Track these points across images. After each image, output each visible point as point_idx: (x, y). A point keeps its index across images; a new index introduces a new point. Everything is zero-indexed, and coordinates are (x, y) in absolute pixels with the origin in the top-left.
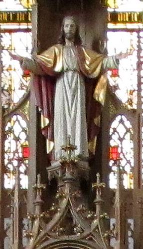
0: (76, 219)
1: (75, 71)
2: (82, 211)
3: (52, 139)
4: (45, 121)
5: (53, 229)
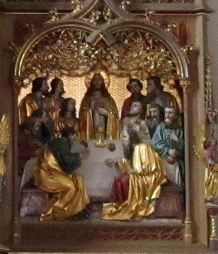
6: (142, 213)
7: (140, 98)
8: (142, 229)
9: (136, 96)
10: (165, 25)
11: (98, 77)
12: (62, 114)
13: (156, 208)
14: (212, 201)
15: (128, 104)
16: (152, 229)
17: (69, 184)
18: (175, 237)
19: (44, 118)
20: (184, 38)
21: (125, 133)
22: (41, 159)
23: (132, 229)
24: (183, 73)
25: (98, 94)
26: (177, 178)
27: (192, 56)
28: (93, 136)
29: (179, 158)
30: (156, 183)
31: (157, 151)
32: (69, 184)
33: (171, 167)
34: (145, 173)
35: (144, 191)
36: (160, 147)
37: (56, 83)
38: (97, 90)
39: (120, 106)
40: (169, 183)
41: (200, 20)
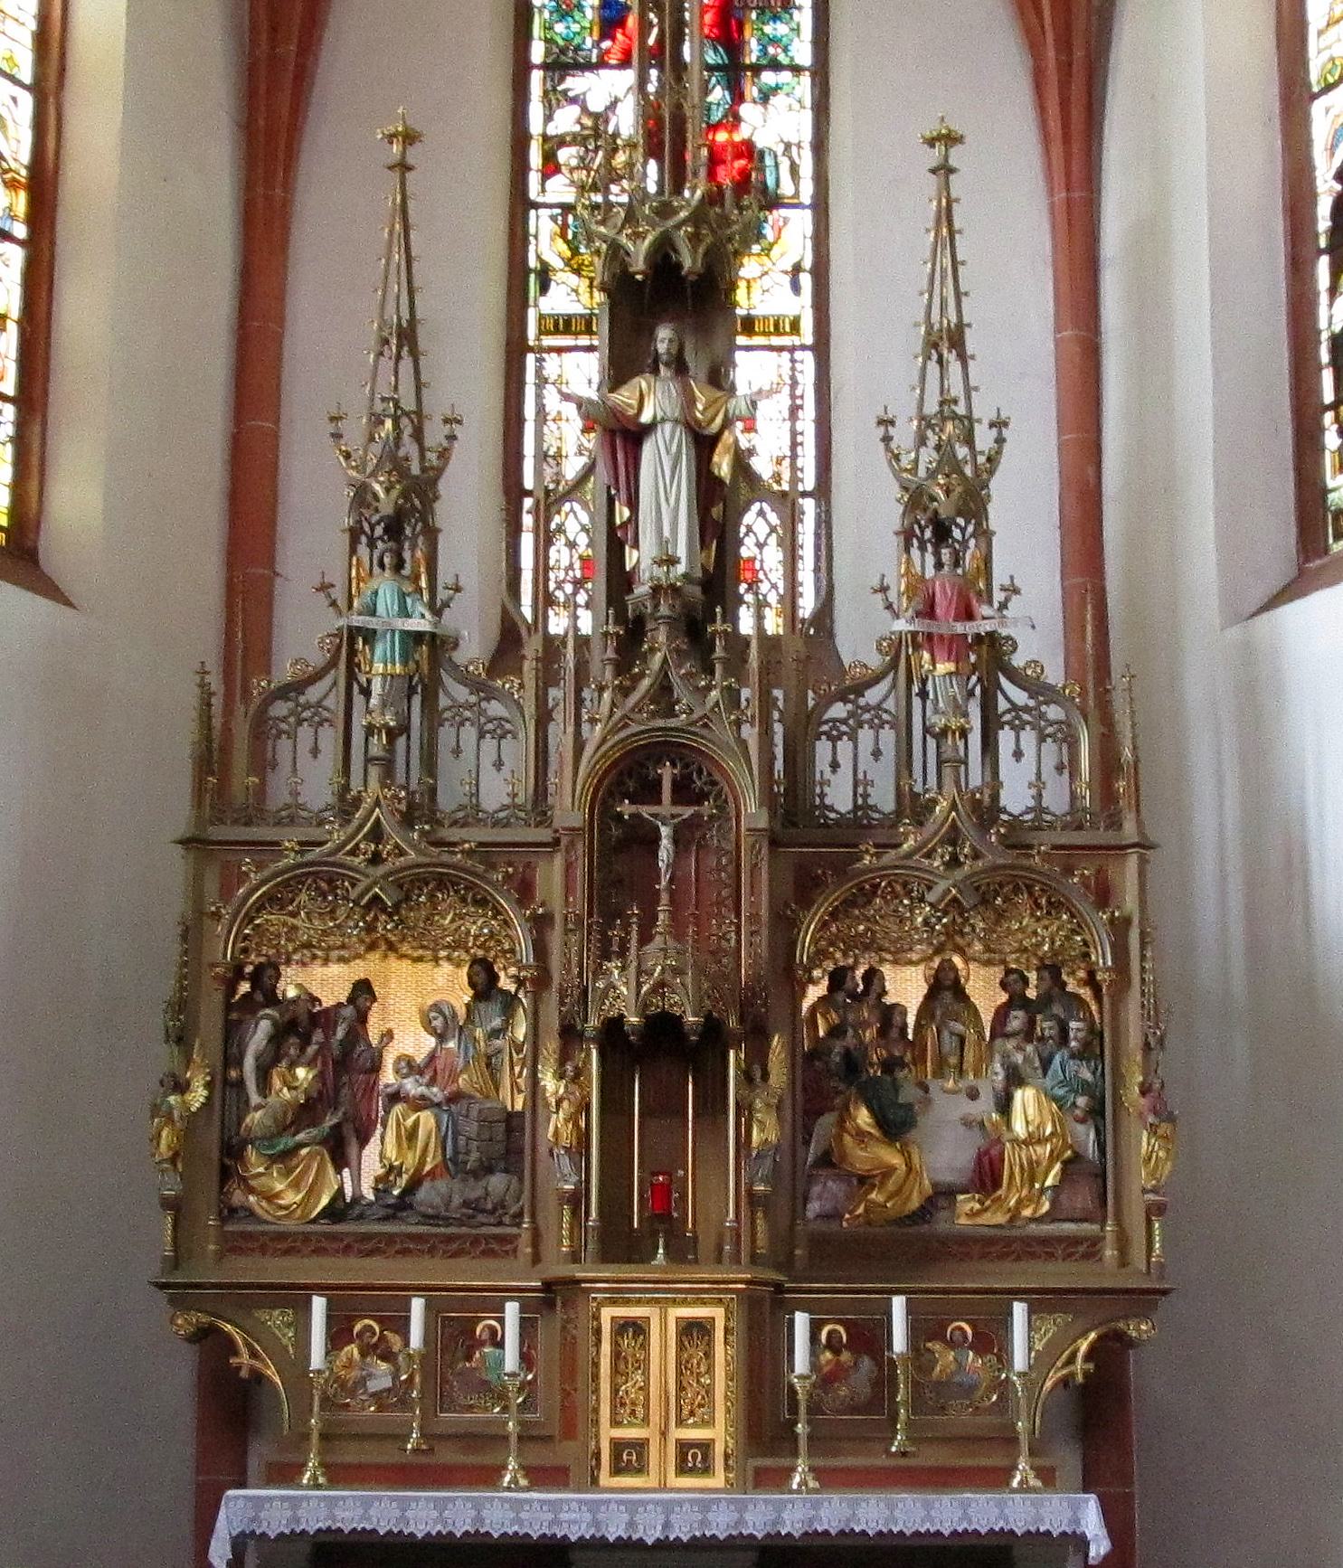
0: (679, 690)
1: (676, 421)
2: (689, 675)
3: (636, 545)
4: (622, 513)
5: (638, 708)
6: (1027, 1212)
7: (1025, 1004)
8: (1028, 1241)
9: (1017, 1000)
10: (1069, 871)
11: (947, 966)
12: (883, 1032)
13: (1053, 1203)
14: (1154, 1191)
15: (1002, 1014)
16: (1045, 1241)
17: (896, 1160)
18: (1087, 1256)
19: (850, 1039)
20: (1103, 895)
21: (998, 1067)
22: (845, 1115)
23: (1009, 1241)
24: (1103, 958)
25: (947, 996)
26: (1091, 1150)
27: (1119, 927)
28: (939, 1073)
29: (1095, 1113)
30: (1053, 1158)
31: (1055, 1099)
32: (896, 1160)
33: (1080, 1128)
34: (1033, 1140)
35: (1032, 1172)
36: (1060, 1092)
37: (872, 975)
38: (945, 989)
39: (987, 1018)
40: (1077, 1157)
41: (1132, 862)
